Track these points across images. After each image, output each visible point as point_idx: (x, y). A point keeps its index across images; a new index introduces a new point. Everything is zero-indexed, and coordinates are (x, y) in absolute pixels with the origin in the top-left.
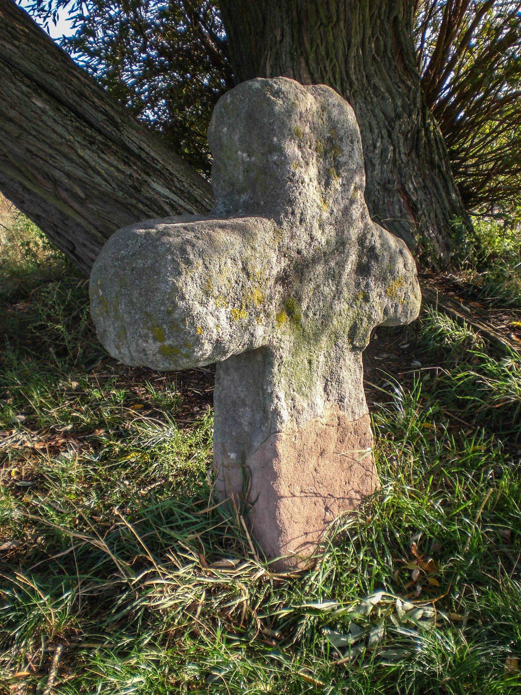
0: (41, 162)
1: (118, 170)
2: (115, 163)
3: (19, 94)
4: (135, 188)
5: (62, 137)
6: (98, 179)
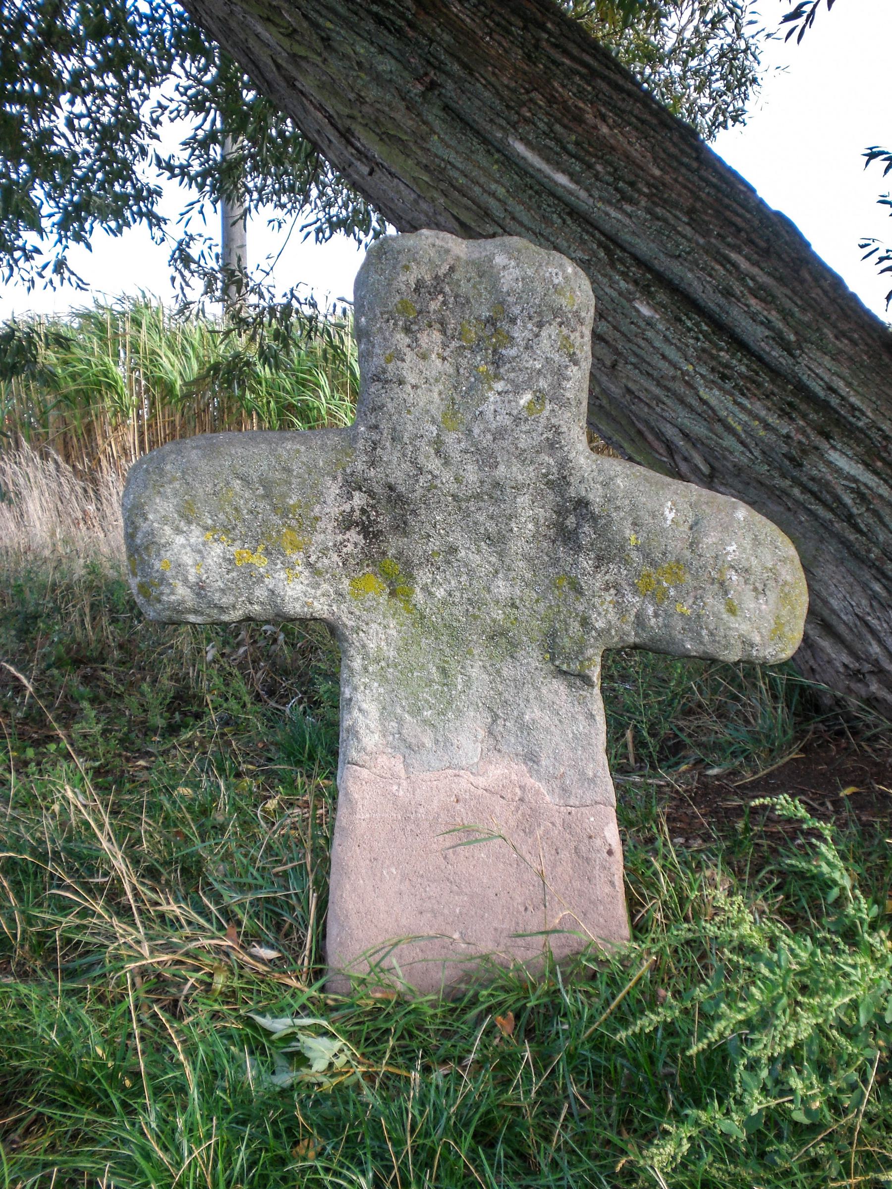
0: (646, 410)
1: (767, 426)
2: (763, 413)
3: (614, 294)
4: (792, 459)
5: (675, 366)
6: (729, 441)
